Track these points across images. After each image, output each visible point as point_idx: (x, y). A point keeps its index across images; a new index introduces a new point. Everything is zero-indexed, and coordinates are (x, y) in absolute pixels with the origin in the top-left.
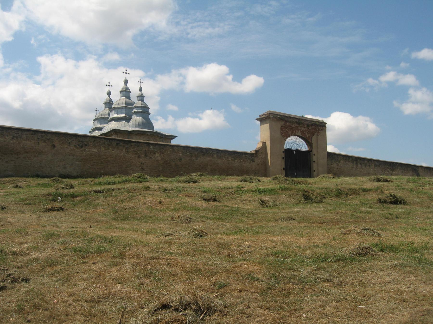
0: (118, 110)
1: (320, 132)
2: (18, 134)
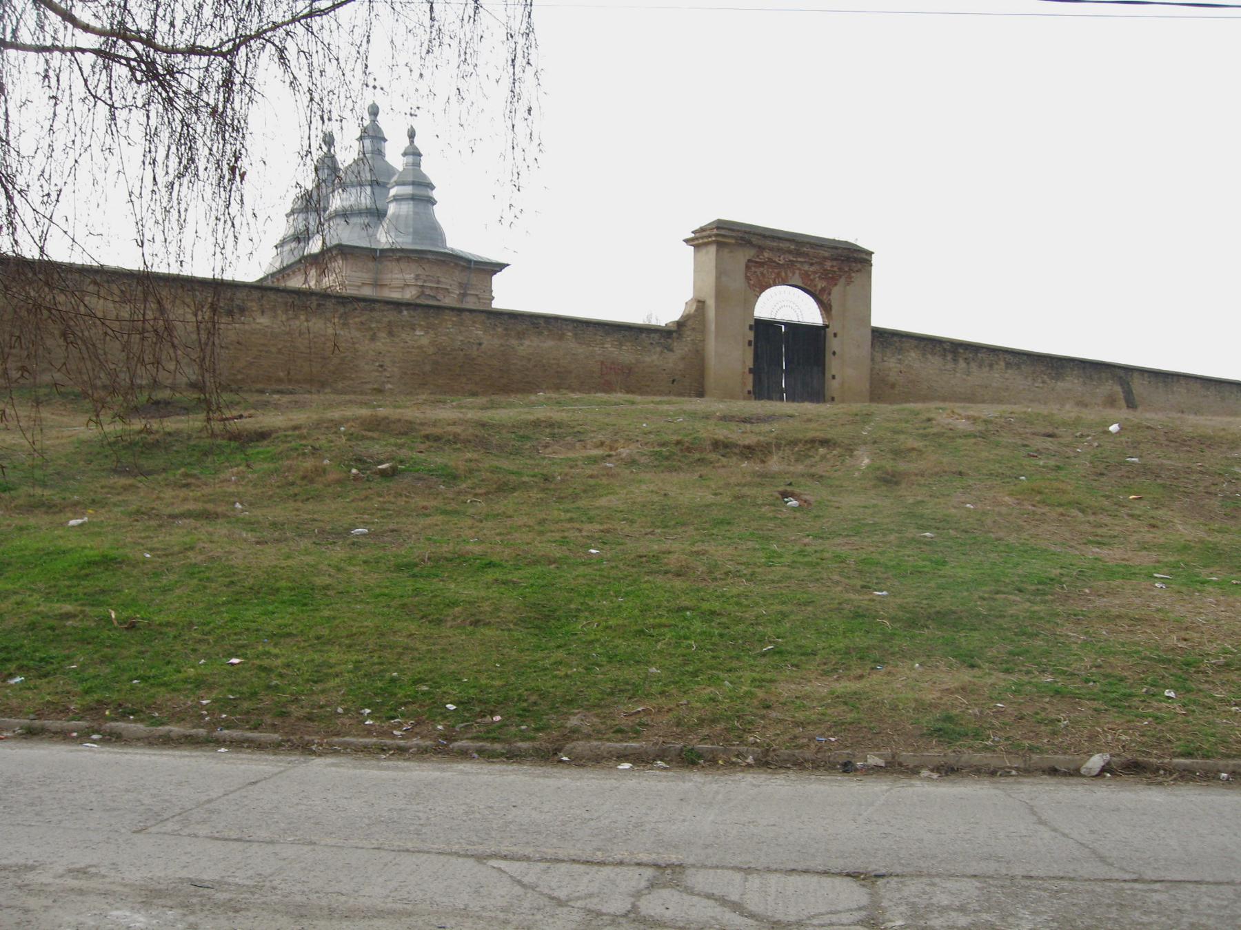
1: (853, 275)
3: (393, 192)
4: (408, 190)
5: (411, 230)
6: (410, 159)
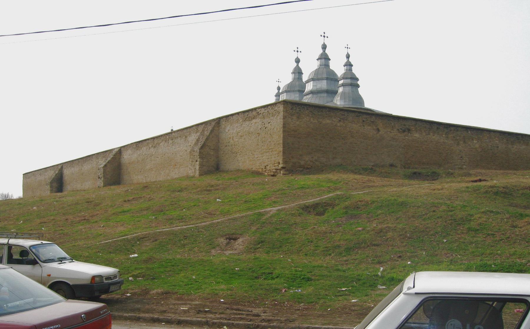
0: (318, 81)
2: (345, 115)
3: (341, 82)
4: (349, 81)
5: (351, 99)
6: (348, 67)
